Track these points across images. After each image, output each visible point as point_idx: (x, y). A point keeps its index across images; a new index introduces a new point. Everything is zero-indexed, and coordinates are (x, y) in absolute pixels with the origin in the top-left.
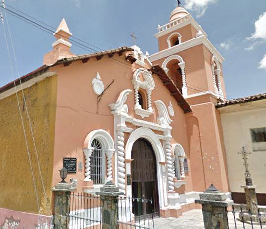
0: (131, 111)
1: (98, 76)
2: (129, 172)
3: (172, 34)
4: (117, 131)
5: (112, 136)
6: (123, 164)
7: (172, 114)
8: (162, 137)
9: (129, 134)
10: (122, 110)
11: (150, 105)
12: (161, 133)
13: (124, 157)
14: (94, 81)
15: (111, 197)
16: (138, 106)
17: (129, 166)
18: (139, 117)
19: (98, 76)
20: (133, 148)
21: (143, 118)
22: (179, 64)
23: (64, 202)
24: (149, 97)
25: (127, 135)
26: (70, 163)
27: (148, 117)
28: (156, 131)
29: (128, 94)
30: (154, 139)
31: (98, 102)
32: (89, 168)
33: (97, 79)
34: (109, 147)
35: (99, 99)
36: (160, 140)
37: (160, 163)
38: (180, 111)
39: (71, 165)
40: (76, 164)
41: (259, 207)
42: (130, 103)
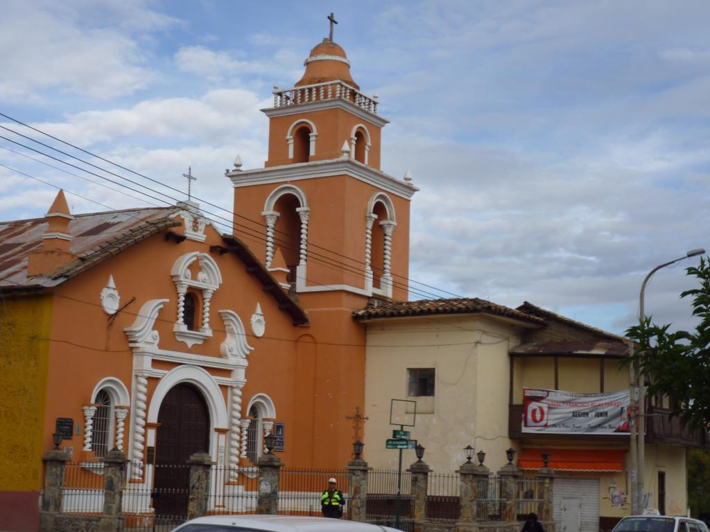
0: (168, 342)
1: (112, 283)
2: (151, 442)
3: (299, 199)
4: (137, 376)
5: (126, 385)
6: (142, 430)
7: (259, 330)
8: (225, 380)
9: (158, 379)
10: (147, 338)
11: (207, 320)
12: (227, 372)
13: (145, 419)
14: (105, 293)
15: (157, 517)
16: (181, 327)
17: (152, 434)
18: (182, 348)
19: (112, 283)
20: (164, 399)
21: (190, 346)
22: (298, 209)
23: (58, 473)
24: (208, 304)
25: (153, 381)
26: (65, 425)
27: (200, 343)
28: (213, 370)
29: (161, 306)
30: (210, 385)
31: (108, 329)
32: (90, 433)
33: (108, 288)
34: (121, 398)
35: (110, 322)
36: (220, 386)
37: (217, 430)
38: (283, 327)
39: (66, 427)
40: (72, 427)
41: (629, 434)
42: (163, 322)
